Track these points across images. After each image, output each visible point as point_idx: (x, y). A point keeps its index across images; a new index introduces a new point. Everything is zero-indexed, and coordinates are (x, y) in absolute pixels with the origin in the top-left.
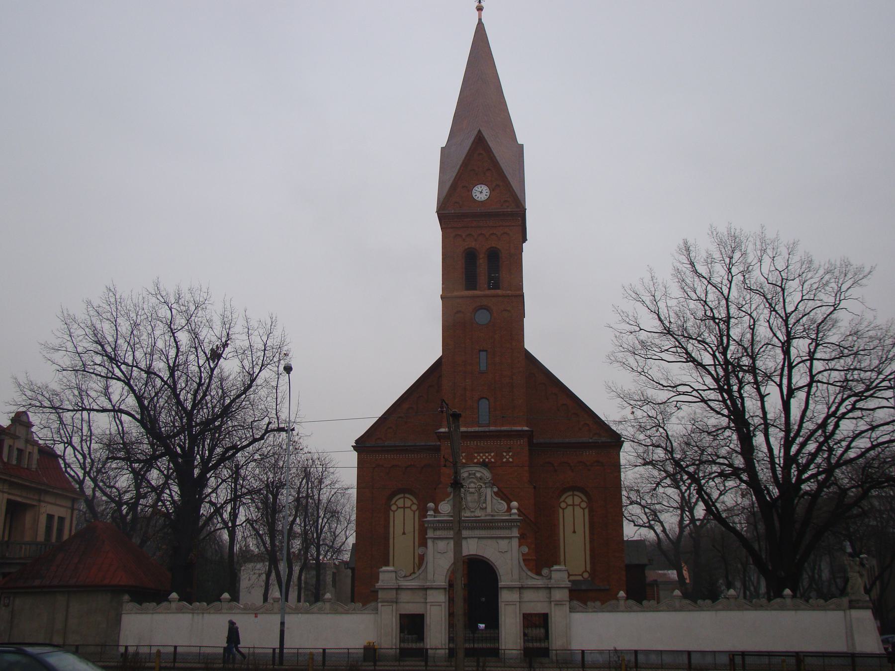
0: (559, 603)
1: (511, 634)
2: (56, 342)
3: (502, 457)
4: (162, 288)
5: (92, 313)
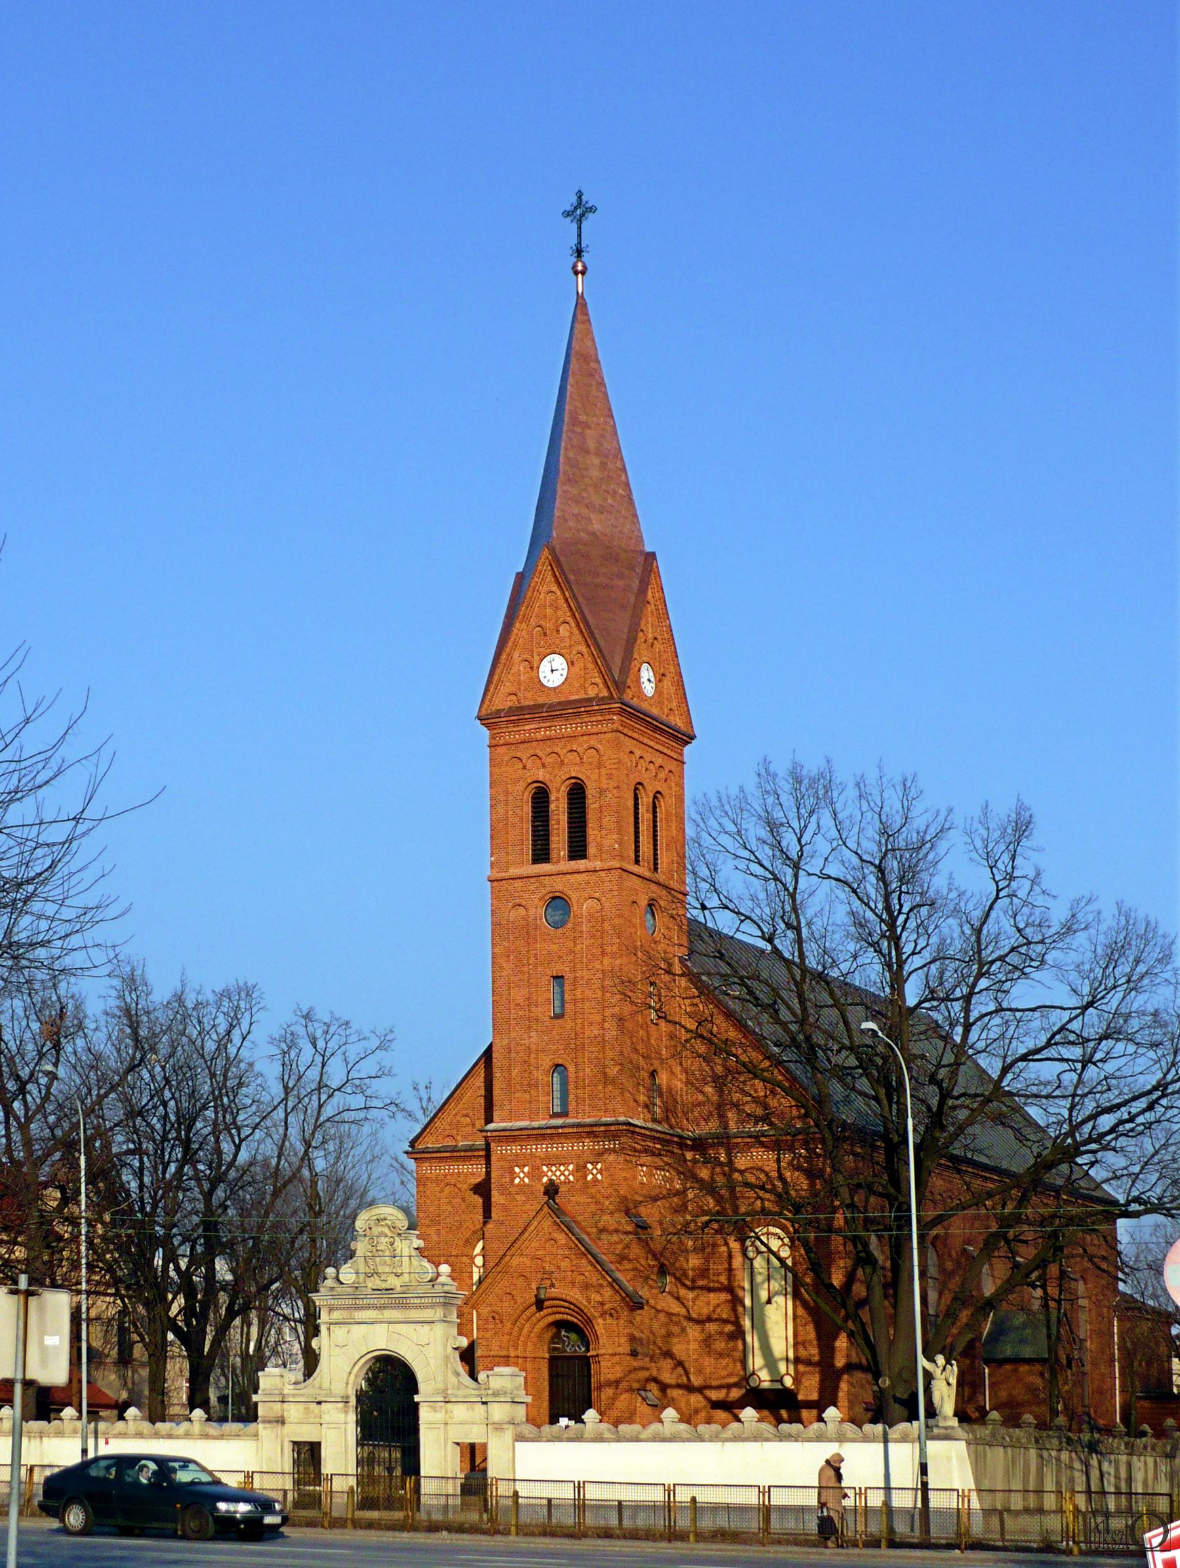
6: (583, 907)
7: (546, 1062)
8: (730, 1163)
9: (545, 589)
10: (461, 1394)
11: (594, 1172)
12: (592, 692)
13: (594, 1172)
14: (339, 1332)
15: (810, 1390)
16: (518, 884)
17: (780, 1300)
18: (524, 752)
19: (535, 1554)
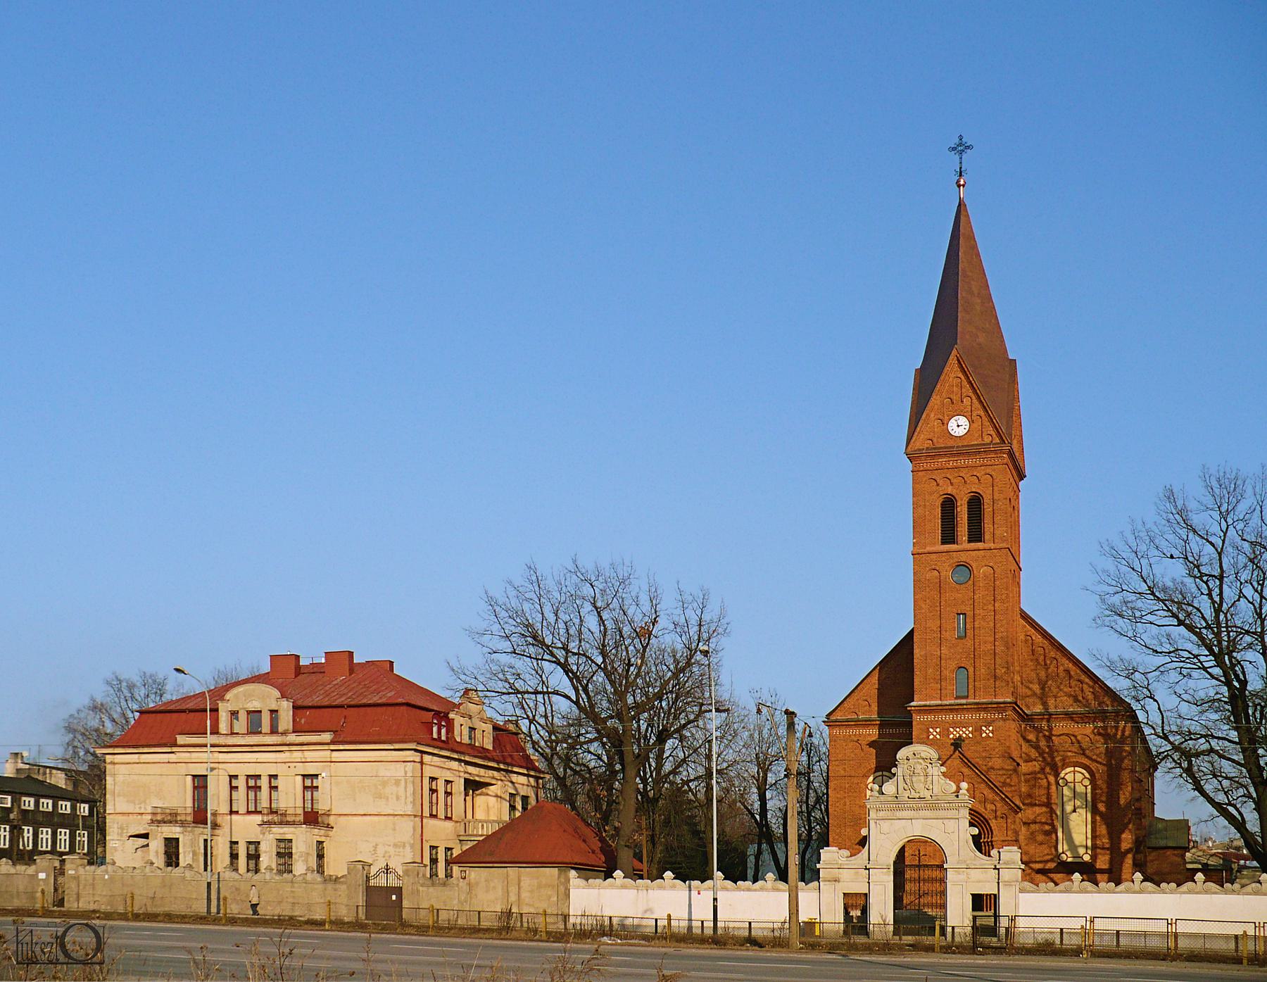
0: (1008, 883)
1: (959, 915)
2: (483, 625)
3: (981, 731)
4: (580, 566)
5: (512, 593)
6: (982, 571)
7: (953, 665)
8: (1050, 729)
9: (952, 375)
10: (978, 863)
11: (987, 732)
12: (987, 440)
13: (987, 732)
14: (885, 825)
15: (1103, 862)
16: (933, 556)
17: (1083, 811)
18: (938, 476)
19: (1128, 975)
